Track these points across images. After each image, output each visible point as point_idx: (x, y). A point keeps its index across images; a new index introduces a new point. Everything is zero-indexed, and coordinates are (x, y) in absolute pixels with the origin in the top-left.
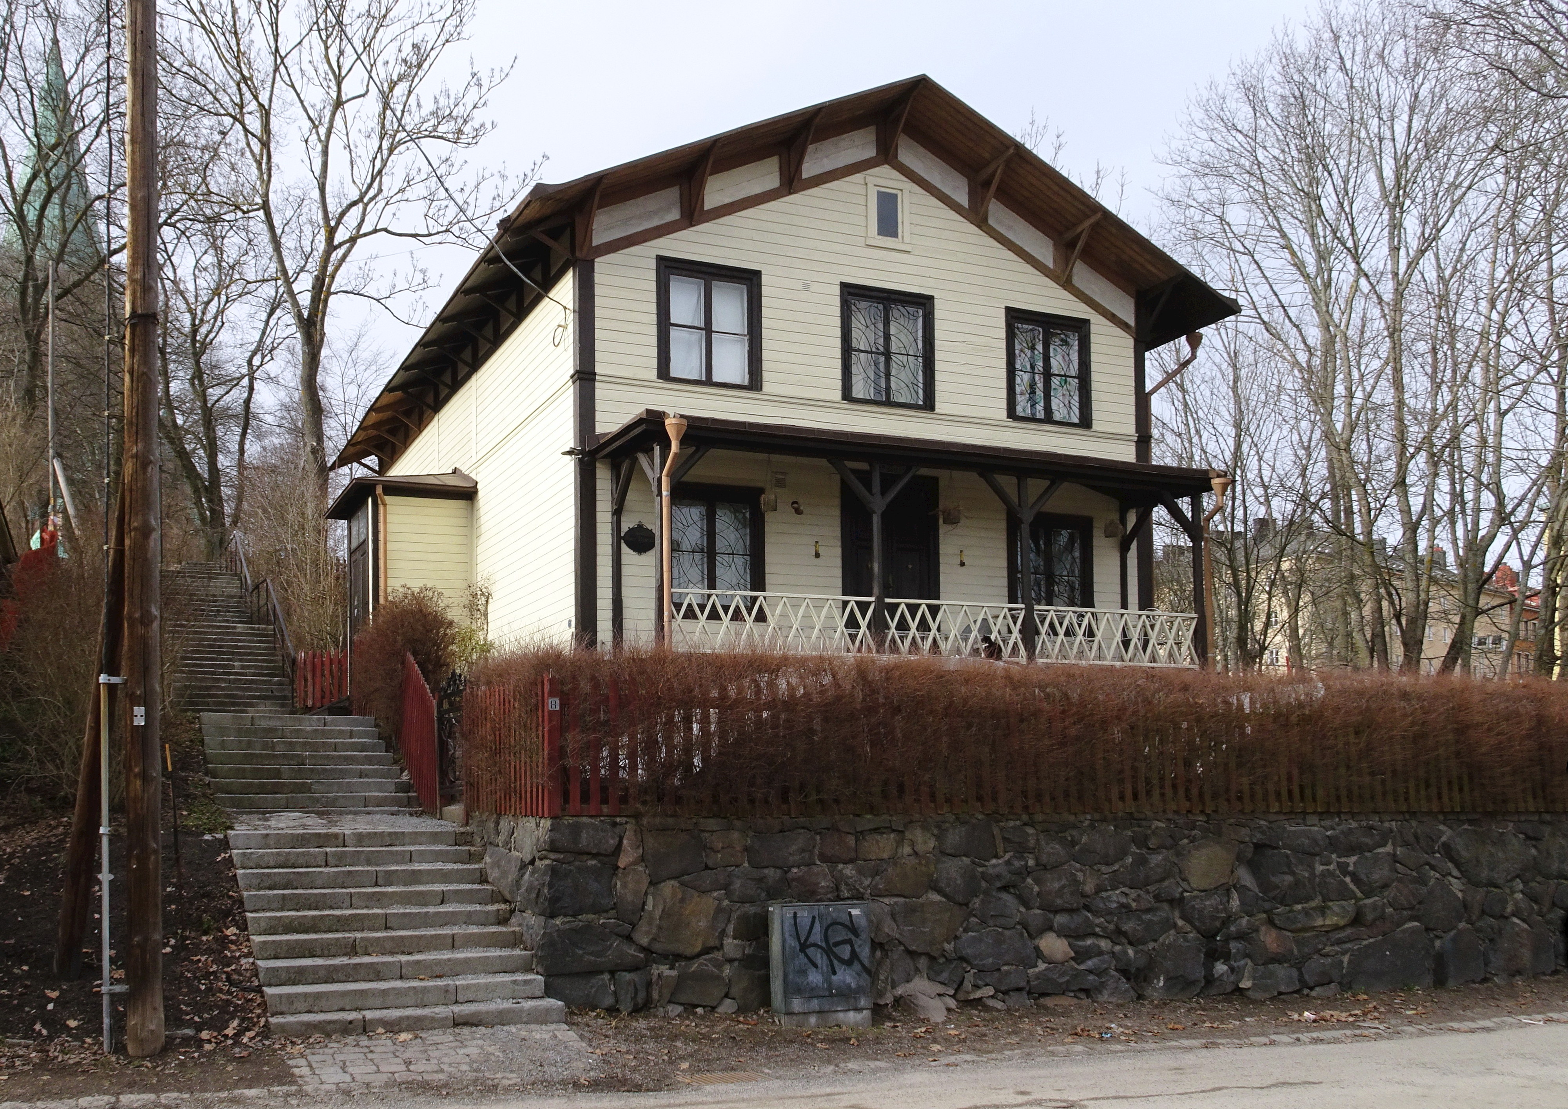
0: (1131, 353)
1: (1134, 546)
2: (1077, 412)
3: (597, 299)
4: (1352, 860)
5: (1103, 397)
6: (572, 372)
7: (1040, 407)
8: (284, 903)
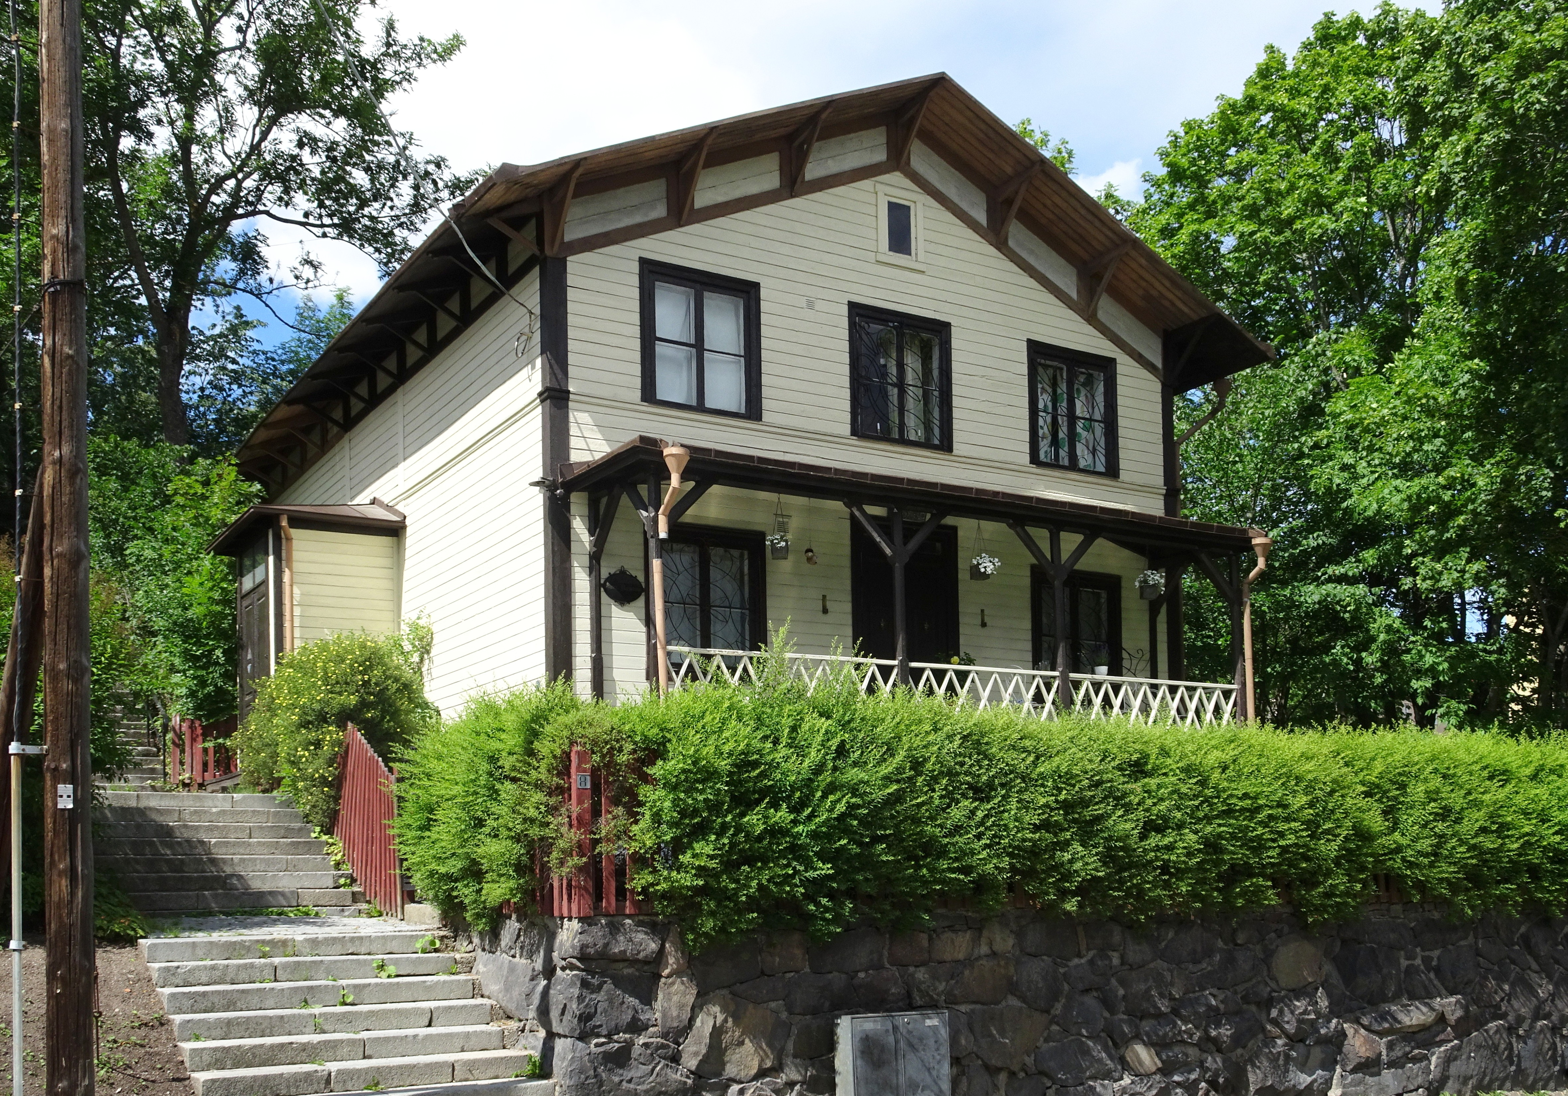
0: (1158, 398)
1: (1164, 610)
2: (1103, 459)
3: (569, 304)
4: (1436, 953)
5: (1131, 444)
6: (539, 388)
7: (1063, 453)
8: (228, 1029)
